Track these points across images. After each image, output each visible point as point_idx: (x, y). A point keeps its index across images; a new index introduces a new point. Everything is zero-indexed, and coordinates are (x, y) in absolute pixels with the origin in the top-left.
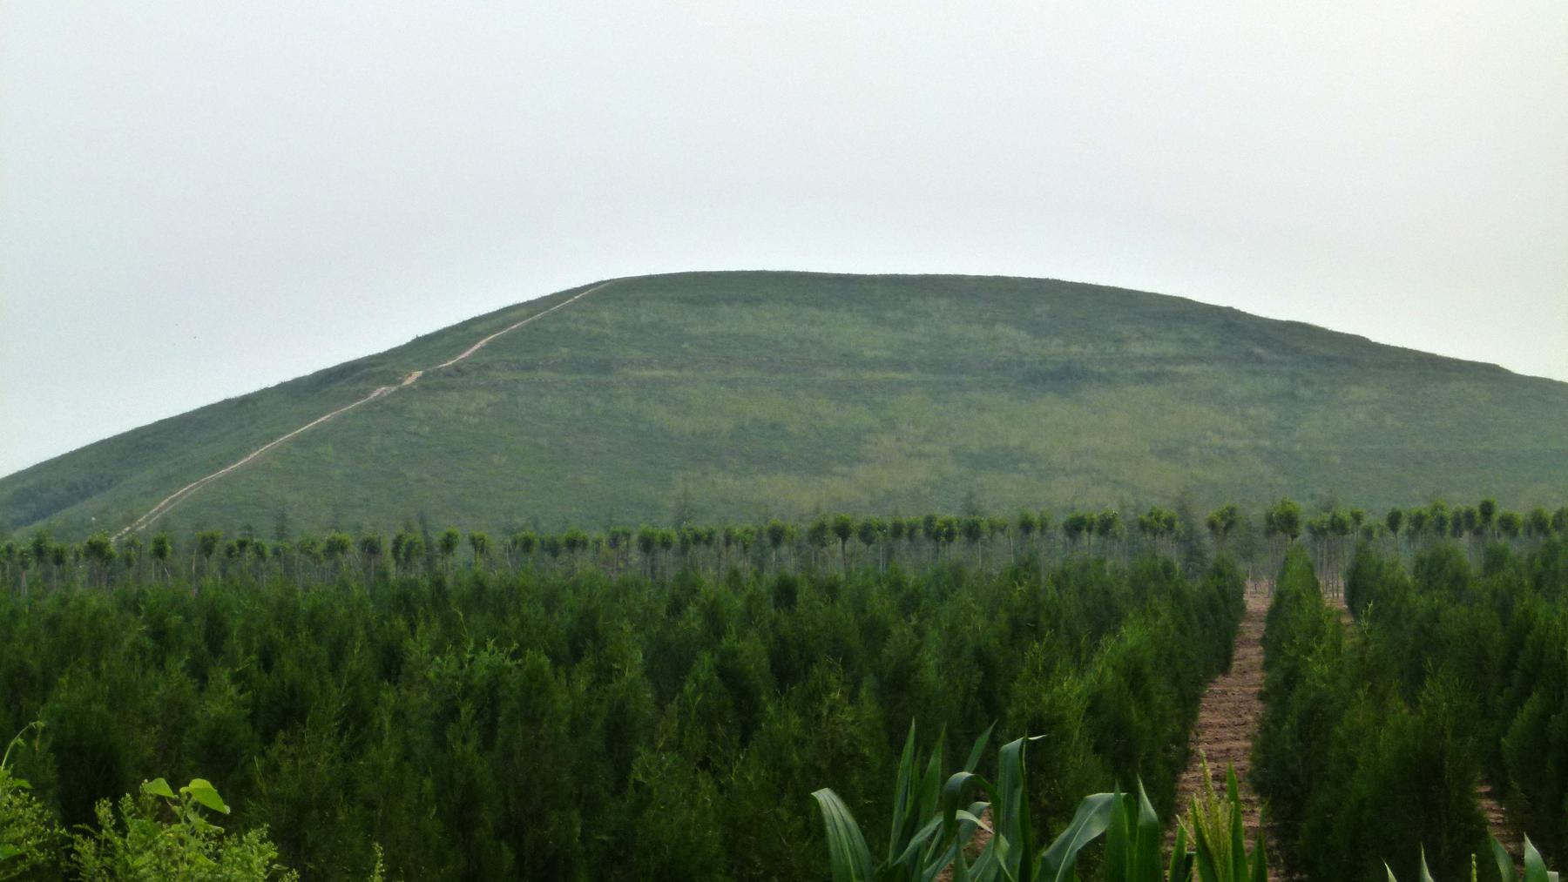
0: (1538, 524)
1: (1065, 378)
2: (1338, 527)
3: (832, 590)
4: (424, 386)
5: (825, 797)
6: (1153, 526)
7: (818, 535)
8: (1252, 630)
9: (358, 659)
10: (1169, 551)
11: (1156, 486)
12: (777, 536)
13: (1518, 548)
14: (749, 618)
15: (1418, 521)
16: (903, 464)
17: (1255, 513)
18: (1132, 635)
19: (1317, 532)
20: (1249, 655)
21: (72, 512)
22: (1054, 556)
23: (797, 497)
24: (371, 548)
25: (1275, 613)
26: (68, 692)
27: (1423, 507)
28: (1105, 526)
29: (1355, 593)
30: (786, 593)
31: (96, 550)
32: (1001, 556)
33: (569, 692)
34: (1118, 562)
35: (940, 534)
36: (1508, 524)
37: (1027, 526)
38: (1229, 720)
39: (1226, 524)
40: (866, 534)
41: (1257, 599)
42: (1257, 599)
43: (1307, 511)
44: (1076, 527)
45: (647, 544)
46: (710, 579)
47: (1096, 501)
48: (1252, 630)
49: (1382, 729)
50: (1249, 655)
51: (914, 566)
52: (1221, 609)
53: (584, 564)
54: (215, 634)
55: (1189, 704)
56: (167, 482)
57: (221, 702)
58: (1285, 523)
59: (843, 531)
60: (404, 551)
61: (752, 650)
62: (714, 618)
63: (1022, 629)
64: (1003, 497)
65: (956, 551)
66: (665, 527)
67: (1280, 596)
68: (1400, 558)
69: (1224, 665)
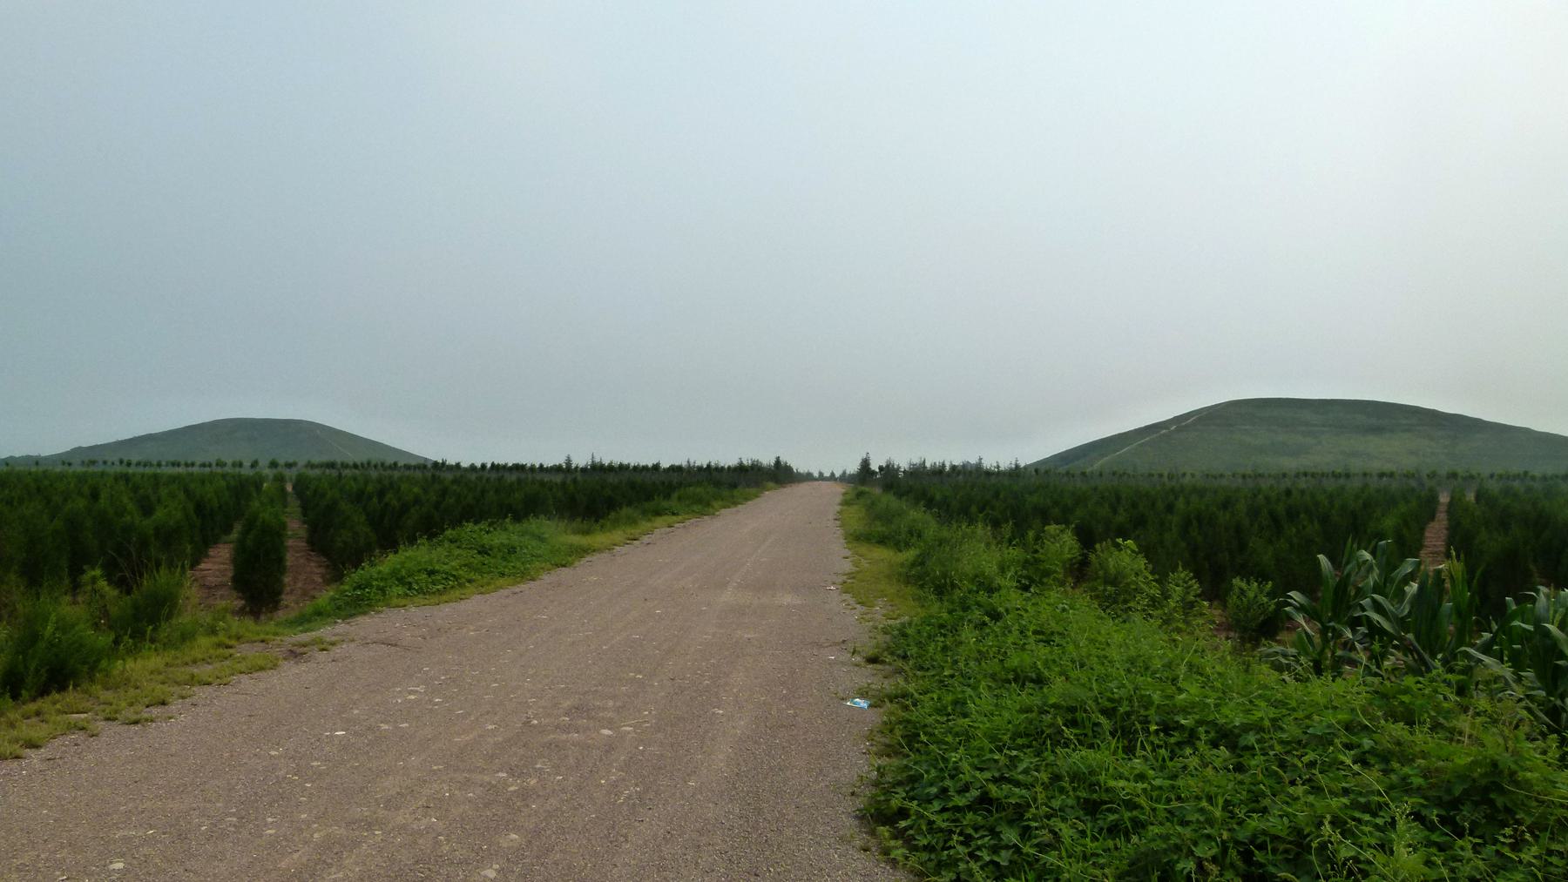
0: (1544, 478)
1: (1377, 430)
2: (1472, 477)
3: (1303, 492)
4: (1177, 430)
5: (1321, 557)
6: (1407, 476)
7: (1297, 475)
8: (1442, 508)
9: (1160, 505)
10: (1413, 483)
11: (1408, 463)
12: (1284, 475)
13: (1537, 485)
14: (1279, 500)
15: (1501, 476)
16: (1324, 455)
17: (1443, 471)
18: (1403, 508)
19: (1464, 479)
20: (1442, 516)
21: (1529, 775)
22: (1374, 484)
23: (1290, 464)
24: (1161, 476)
25: (1451, 504)
26: (1079, 512)
27: (1501, 471)
28: (1391, 475)
29: (1478, 498)
30: (1288, 493)
31: (1083, 474)
32: (1356, 484)
33: (1224, 517)
34: (1395, 486)
35: (1336, 476)
36: (1533, 478)
37: (1365, 474)
38: (1436, 533)
39: (1432, 476)
40: (1313, 475)
41: (1444, 498)
42: (1444, 498)
43: (1460, 471)
44: (1381, 475)
45: (1244, 477)
46: (1264, 486)
47: (1388, 467)
48: (1442, 508)
49: (1492, 543)
50: (1442, 516)
51: (1330, 485)
52: (1431, 502)
53: (1224, 482)
54: (1118, 498)
55: (1422, 530)
56: (1103, 456)
57: (1121, 517)
58: (1454, 475)
59: (1305, 474)
60: (1170, 477)
61: (1280, 509)
62: (1267, 498)
63: (1366, 505)
64: (1356, 465)
65: (1342, 481)
66: (1249, 472)
67: (1452, 498)
68: (1494, 487)
69: (1432, 518)
